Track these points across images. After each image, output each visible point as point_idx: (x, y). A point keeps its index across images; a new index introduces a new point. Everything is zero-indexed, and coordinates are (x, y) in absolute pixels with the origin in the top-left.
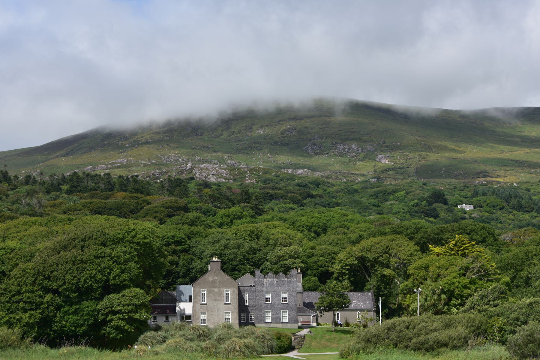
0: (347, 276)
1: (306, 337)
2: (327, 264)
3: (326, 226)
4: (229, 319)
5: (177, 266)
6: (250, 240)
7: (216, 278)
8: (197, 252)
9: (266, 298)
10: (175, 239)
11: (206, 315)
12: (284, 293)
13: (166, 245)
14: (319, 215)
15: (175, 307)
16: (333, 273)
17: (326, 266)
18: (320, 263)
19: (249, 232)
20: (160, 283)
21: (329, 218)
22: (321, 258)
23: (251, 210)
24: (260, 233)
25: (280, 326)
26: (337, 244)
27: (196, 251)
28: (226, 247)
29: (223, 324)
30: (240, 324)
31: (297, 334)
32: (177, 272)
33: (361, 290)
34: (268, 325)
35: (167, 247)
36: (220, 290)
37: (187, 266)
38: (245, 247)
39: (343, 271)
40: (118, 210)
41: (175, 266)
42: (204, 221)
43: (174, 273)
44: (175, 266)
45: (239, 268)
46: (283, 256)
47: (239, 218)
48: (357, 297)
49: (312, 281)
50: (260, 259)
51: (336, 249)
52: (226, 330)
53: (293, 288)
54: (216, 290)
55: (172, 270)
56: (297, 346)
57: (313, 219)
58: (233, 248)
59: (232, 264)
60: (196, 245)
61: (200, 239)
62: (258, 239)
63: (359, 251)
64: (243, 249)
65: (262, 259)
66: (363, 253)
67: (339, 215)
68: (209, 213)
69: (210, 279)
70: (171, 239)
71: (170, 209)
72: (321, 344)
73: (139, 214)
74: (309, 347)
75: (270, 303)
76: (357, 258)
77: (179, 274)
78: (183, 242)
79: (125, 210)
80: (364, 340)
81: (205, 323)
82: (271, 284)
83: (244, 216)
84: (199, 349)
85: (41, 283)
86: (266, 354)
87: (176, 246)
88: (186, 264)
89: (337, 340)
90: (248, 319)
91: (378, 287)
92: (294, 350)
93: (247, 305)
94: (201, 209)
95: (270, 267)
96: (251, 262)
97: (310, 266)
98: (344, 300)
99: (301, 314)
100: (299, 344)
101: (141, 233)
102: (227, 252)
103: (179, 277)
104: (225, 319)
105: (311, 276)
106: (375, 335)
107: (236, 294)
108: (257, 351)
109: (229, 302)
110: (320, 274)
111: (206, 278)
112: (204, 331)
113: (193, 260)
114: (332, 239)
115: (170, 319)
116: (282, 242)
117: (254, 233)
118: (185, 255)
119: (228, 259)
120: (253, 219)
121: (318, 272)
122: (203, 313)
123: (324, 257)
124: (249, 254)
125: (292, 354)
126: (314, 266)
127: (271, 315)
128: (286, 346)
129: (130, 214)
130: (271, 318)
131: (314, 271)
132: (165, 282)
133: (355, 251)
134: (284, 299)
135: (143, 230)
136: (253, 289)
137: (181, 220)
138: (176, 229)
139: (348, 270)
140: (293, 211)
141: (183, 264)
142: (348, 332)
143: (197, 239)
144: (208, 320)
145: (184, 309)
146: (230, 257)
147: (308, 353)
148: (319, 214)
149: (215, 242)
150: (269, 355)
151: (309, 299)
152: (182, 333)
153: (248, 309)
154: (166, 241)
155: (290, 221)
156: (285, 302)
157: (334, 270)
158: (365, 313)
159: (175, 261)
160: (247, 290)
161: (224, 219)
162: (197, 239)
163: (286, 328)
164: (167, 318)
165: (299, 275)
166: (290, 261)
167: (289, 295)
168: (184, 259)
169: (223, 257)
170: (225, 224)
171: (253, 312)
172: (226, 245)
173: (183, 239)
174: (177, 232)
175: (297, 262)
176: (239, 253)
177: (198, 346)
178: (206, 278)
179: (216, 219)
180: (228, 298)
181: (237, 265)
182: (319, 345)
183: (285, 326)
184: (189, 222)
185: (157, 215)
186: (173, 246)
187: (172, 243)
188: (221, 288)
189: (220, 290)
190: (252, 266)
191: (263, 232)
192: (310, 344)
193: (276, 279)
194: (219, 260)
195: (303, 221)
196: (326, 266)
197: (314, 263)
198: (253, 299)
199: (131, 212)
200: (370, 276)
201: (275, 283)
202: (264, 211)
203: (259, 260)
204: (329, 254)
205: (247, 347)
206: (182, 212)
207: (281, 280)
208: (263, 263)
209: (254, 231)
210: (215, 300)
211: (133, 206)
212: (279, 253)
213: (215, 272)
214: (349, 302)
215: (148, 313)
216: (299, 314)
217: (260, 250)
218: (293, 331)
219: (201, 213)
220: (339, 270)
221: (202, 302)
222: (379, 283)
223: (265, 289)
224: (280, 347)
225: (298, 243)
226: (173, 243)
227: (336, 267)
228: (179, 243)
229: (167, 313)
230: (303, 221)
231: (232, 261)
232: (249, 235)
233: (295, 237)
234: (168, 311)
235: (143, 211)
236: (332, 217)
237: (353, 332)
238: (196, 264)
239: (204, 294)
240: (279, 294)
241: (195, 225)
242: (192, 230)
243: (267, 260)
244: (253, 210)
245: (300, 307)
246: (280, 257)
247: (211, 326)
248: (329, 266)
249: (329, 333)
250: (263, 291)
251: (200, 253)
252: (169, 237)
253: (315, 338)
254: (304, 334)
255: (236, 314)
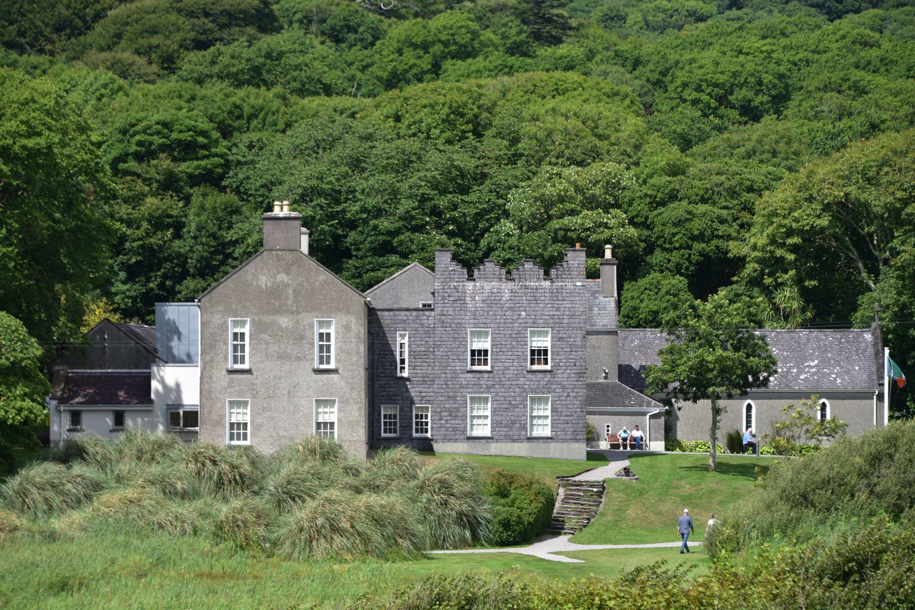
0: (792, 273)
1: (609, 489)
2: (722, 229)
3: (787, 86)
4: (332, 424)
5: (177, 235)
6: (449, 142)
7: (282, 277)
8: (254, 184)
9: (473, 352)
10: (174, 136)
11: (248, 410)
12: (540, 334)
13: (139, 157)
14: (765, 45)
15: (147, 379)
16: (741, 262)
17: (718, 237)
18: (696, 226)
19: (446, 110)
20: (116, 294)
21: (800, 56)
22: (702, 208)
23: (518, 22)
24: (485, 115)
25: (521, 449)
26: (774, 154)
27: (248, 178)
28: (356, 164)
29: (307, 441)
30: (375, 443)
31: (577, 479)
32: (179, 255)
33: (842, 322)
34: (478, 449)
35: (144, 165)
36: (297, 322)
37: (213, 236)
38: (429, 166)
39: (779, 253)
40: (11, 23)
41: (169, 233)
42: (298, 67)
43: (169, 259)
44: (169, 233)
45: (401, 243)
46: (561, 200)
47: (465, 53)
48: (819, 348)
49: (664, 290)
50: (485, 212)
51: (756, 173)
52: (315, 463)
53: (572, 316)
54: (284, 321)
55: (160, 247)
56: (572, 521)
57: (742, 58)
58: (385, 169)
59: (375, 227)
60: (250, 158)
61: (265, 135)
62: (478, 135)
63: (841, 182)
64: (421, 174)
65: (492, 210)
66: (848, 189)
67: (840, 44)
68: (352, 36)
69: (264, 281)
70: (158, 133)
71: (203, 20)
72: (659, 513)
73: (90, 37)
74: (616, 523)
75: (488, 368)
76: (827, 208)
77: (186, 262)
78: (204, 147)
79: (39, 23)
80: (788, 499)
81: (245, 438)
82: (492, 301)
83: (484, 45)
84: (207, 526)
85: (640, 352)
86: (455, 548)
87: (175, 160)
88: (212, 228)
89: (718, 498)
90: (407, 427)
91: (902, 310)
92: (560, 534)
93: (405, 374)
94: (323, 21)
95: (513, 241)
96: (448, 221)
97: (658, 238)
98: (748, 356)
99: (609, 409)
100: (579, 513)
101: (15, 115)
102: (359, 182)
103: (184, 275)
104: (318, 425)
105: (662, 272)
106: (827, 482)
107: (358, 336)
108: (413, 535)
109: (332, 366)
110: (698, 264)
111: (249, 277)
112: (233, 467)
113: (237, 211)
114: (755, 137)
115: (129, 422)
116: (567, 147)
117: (462, 115)
118: (205, 195)
119: (364, 210)
120: (511, 60)
121: (688, 259)
122: (238, 404)
123: (714, 203)
124: (443, 192)
125: (543, 550)
126: (674, 235)
127: (488, 413)
128: (528, 519)
129: (55, 36)
130: (489, 421)
131: (675, 253)
132: (135, 289)
133: (824, 181)
134: (539, 355)
135: (26, 103)
136: (429, 319)
137: (213, 63)
138: (180, 96)
139: (794, 249)
140: (701, 25)
141: (200, 229)
142: (745, 470)
143: (254, 136)
144: (257, 428)
145: (178, 386)
146: (371, 202)
147: (606, 543)
148: (764, 38)
149: (320, 146)
150: (464, 551)
151: (645, 354)
152: (155, 470)
153: (407, 390)
154: (140, 143)
155: (651, 66)
156: (542, 367)
157: (745, 250)
158: (809, 402)
159: (170, 216)
160: (404, 322)
161: (409, 56)
162: (254, 136)
163: (544, 460)
164: (119, 420)
165: (607, 268)
166: (584, 218)
167: (557, 339)
168: (202, 207)
169: (347, 199)
170: (409, 76)
171: (429, 402)
172: (358, 160)
173: (204, 133)
174: (180, 109)
175: (612, 223)
176: (404, 186)
177: (204, 515)
178: (249, 277)
179: (377, 56)
180: (328, 351)
181: (398, 232)
182: (652, 517)
183: (538, 451)
184: (242, 71)
185: (155, 40)
186: (164, 162)
187: (163, 148)
188: (303, 315)
189: (297, 322)
190: (451, 234)
191: (498, 109)
192: (620, 513)
193: (510, 285)
194: (294, 214)
195: (701, 67)
196: (718, 237)
197: (675, 225)
198: (426, 354)
199: (59, 29)
200: (874, 271)
201: (507, 296)
202: (571, 28)
203: (479, 216)
204: (733, 193)
205: (378, 521)
206: (250, 30)
207: (526, 287)
208: (492, 226)
209: (465, 105)
210: (283, 357)
211: (68, 7)
212: (549, 190)
213: (279, 258)
214: (770, 365)
215: (33, 401)
216: (591, 408)
217: (484, 176)
218: (563, 470)
219: (323, 33)
220: (763, 249)
221: (235, 362)
222: (904, 298)
223: (468, 318)
224: (506, 524)
225: (625, 153)
226: (163, 152)
227: (753, 240)
228: (187, 150)
229: (120, 403)
230: (701, 67)
231: (376, 217)
232: (444, 121)
233: (617, 131)
234: (121, 393)
235: (104, 27)
236: (814, 52)
237: (765, 470)
238: (247, 226)
239: (243, 334)
240: (519, 338)
241: (265, 82)
242: (239, 102)
243: (506, 214)
244: (524, 22)
245: (607, 385)
246: (548, 204)
247: (266, 449)
248: (729, 238)
249: (695, 475)
250: (460, 326)
251: (263, 186)
252: (150, 127)
253: (641, 493)
254: (601, 479)
255: (355, 407)
